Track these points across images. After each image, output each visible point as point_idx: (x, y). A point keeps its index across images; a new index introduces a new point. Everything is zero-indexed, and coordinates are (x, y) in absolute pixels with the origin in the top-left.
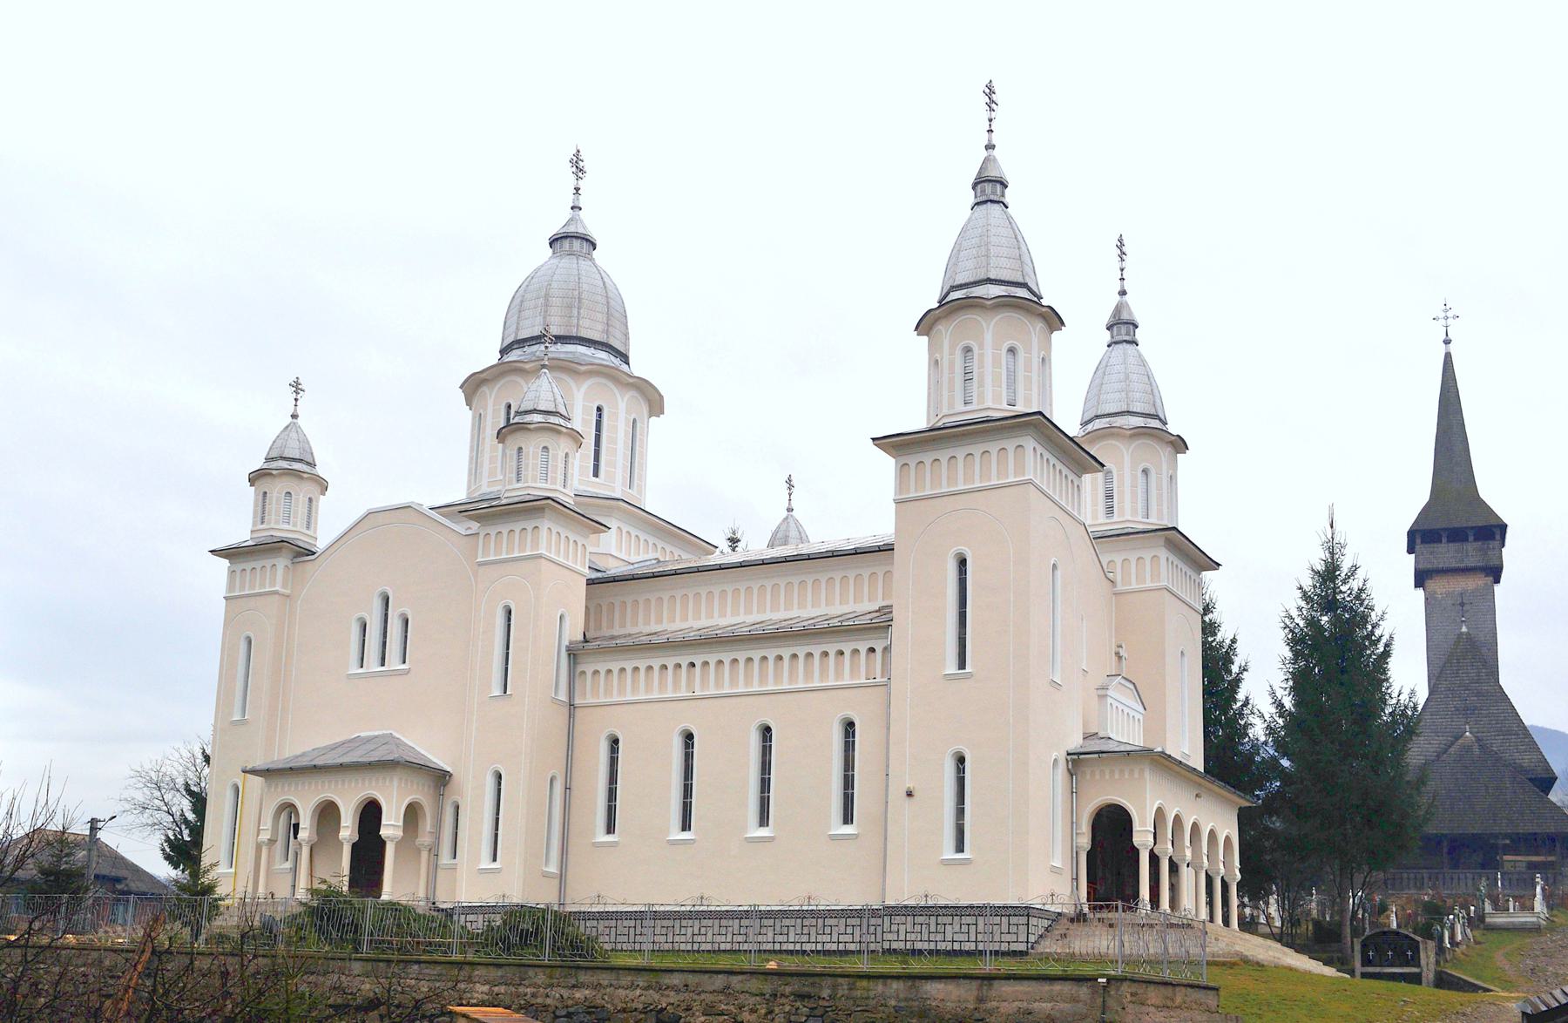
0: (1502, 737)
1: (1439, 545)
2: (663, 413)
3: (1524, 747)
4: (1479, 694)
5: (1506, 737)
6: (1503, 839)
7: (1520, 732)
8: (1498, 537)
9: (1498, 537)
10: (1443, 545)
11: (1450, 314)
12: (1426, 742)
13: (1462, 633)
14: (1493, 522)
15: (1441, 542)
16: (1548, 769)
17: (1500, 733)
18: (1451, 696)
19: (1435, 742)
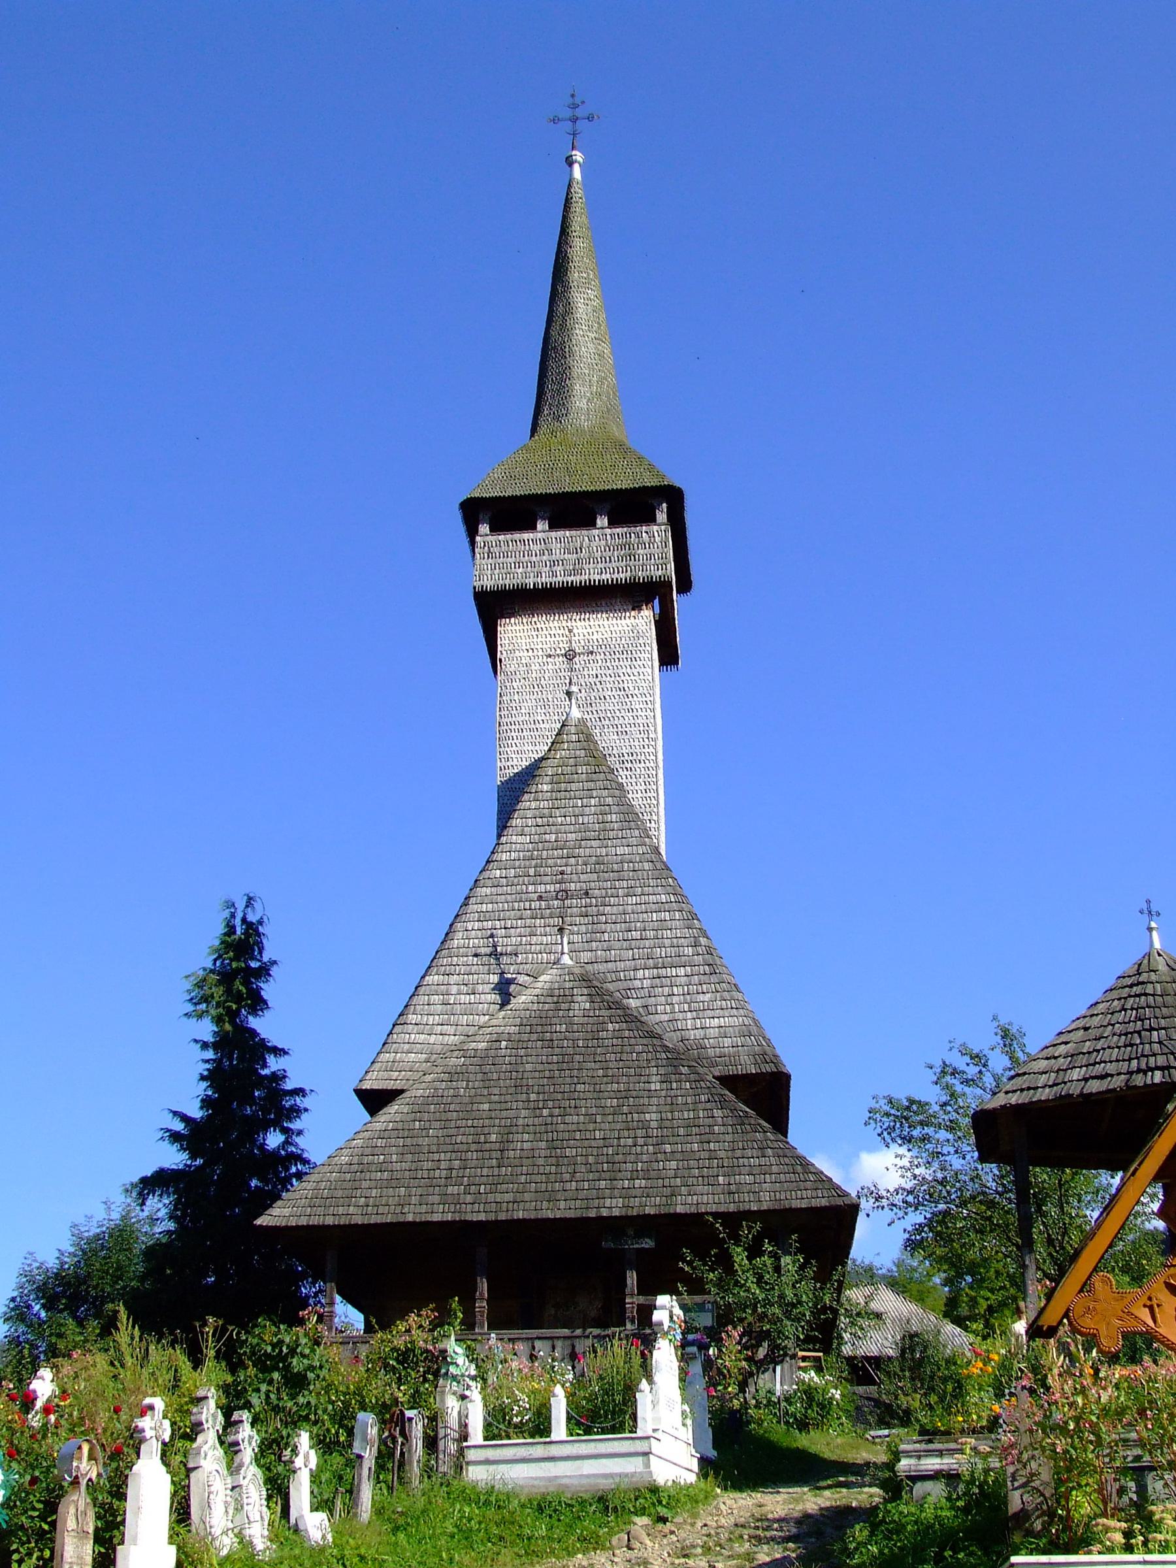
1: (526, 536)
5: (663, 972)
6: (640, 1235)
8: (662, 516)
9: (662, 516)
11: (579, 112)
16: (775, 1060)
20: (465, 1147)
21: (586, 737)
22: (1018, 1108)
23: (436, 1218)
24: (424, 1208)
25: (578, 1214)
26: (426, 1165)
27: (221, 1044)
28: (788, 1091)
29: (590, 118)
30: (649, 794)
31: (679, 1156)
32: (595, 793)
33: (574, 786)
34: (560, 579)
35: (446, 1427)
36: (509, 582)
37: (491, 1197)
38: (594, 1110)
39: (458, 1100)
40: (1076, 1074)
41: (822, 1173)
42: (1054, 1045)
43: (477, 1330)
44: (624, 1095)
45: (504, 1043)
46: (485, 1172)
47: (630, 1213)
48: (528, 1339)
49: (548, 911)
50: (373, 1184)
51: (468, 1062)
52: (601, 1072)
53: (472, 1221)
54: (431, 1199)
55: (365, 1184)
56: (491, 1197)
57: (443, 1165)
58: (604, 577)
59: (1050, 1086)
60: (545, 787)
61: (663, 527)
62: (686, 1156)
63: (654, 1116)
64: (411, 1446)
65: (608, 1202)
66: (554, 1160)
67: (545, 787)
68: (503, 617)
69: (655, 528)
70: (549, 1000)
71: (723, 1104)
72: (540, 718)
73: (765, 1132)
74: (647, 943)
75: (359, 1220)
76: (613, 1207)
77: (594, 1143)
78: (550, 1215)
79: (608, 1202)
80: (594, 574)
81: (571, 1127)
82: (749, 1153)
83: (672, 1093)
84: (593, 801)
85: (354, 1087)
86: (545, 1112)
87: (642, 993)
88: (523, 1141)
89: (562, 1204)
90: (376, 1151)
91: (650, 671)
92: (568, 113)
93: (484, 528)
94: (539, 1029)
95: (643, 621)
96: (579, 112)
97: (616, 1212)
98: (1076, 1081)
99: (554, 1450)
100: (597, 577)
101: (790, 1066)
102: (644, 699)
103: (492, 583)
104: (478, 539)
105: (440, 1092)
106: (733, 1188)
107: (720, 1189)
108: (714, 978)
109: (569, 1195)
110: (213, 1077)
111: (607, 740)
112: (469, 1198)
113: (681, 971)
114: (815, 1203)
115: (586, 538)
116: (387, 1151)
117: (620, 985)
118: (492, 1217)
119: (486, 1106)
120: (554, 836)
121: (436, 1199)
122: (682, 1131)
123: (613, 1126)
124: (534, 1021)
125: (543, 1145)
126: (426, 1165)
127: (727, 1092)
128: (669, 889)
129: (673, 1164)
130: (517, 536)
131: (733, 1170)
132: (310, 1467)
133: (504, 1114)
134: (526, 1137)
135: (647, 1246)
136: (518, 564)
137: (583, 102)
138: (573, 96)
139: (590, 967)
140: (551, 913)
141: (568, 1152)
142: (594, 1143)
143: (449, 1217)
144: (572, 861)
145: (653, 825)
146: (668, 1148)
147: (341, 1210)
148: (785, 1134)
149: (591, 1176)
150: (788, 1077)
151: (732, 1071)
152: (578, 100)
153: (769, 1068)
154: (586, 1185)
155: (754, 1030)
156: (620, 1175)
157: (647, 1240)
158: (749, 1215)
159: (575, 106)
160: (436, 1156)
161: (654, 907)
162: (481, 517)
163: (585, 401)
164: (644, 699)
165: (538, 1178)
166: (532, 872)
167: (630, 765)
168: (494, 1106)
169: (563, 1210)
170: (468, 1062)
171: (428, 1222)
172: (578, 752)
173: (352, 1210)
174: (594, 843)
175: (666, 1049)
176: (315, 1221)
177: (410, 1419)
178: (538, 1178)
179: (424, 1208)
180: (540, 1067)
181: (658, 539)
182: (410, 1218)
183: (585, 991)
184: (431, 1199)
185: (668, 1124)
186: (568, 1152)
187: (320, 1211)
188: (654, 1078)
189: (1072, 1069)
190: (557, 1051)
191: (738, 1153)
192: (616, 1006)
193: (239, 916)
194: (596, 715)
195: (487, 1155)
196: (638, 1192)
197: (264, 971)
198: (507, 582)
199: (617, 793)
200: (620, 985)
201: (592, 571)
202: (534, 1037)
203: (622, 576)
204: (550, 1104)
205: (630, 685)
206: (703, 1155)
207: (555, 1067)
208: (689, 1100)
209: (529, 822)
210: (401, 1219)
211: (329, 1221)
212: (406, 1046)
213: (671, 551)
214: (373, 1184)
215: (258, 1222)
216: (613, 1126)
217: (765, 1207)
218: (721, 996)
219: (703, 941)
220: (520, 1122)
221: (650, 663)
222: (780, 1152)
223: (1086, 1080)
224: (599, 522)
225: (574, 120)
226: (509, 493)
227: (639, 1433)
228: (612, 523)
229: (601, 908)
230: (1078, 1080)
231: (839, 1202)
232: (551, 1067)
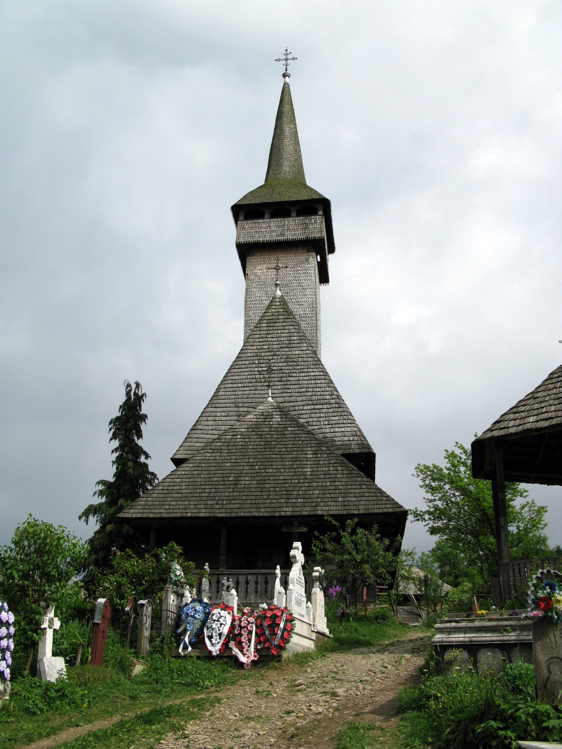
3: (336, 418)
4: (288, 359)
5: (316, 407)
6: (300, 525)
7: (333, 401)
8: (321, 213)
10: (265, 220)
11: (289, 57)
12: (223, 414)
14: (315, 197)
16: (368, 447)
17: (310, 402)
20: (217, 483)
21: (283, 302)
22: (499, 437)
23: (202, 515)
24: (196, 511)
25: (270, 514)
26: (198, 491)
27: (121, 447)
28: (374, 463)
29: (293, 59)
30: (313, 332)
31: (319, 488)
32: (287, 328)
33: (277, 324)
34: (274, 238)
35: (167, 610)
36: (251, 240)
37: (228, 506)
38: (280, 467)
39: (216, 461)
40: (531, 419)
41: (389, 496)
42: (517, 407)
43: (220, 570)
44: (296, 459)
45: (239, 436)
46: (226, 494)
47: (295, 514)
48: (245, 574)
49: (263, 379)
50: (173, 499)
51: (222, 444)
52: (284, 450)
53: (219, 517)
54: (200, 506)
55: (169, 499)
56: (228, 506)
57: (207, 491)
58: (294, 237)
59: (516, 426)
60: (264, 325)
61: (321, 217)
62: (324, 488)
63: (309, 470)
64: (142, 621)
65: (284, 509)
66: (259, 489)
67: (264, 325)
68: (249, 255)
69: (317, 217)
70: (261, 417)
71: (342, 464)
72: (264, 299)
73: (362, 477)
74: (309, 394)
75: (164, 515)
76: (287, 511)
77: (279, 482)
78: (256, 514)
79: (284, 509)
80: (289, 236)
81: (268, 474)
82: (354, 487)
83: (318, 459)
84: (286, 331)
85: (171, 457)
86: (257, 467)
87: (305, 416)
88: (245, 481)
89: (262, 510)
90: (176, 484)
91: (314, 278)
92: (284, 57)
93: (241, 217)
94: (256, 430)
95: (314, 260)
96: (289, 57)
97: (288, 514)
98: (531, 422)
100: (291, 238)
101: (375, 451)
102: (311, 290)
103: (244, 241)
104: (239, 222)
105: (208, 458)
106: (346, 503)
107: (339, 504)
108: (340, 410)
109: (266, 505)
110: (120, 461)
111: (293, 307)
112: (218, 506)
113: (325, 406)
114: (385, 511)
115: (287, 222)
116: (181, 484)
117: (296, 413)
118: (229, 515)
119: (229, 464)
120: (267, 346)
121: (202, 506)
122: (322, 477)
123: (289, 474)
124: (254, 426)
125: (255, 482)
126: (198, 491)
127: (344, 459)
128: (320, 370)
129: (317, 492)
130: (255, 221)
131: (345, 495)
132: (54, 627)
133: (237, 468)
134: (247, 478)
135: (304, 531)
136: (256, 232)
137: (290, 53)
138: (286, 50)
139: (281, 404)
140: (264, 380)
141: (266, 486)
142: (279, 482)
143: (208, 515)
144: (275, 357)
145: (314, 345)
146: (315, 484)
147: (157, 511)
148: (374, 481)
149: (277, 497)
150: (374, 455)
151: (347, 451)
152: (288, 52)
153: (365, 450)
154: (275, 501)
155: (358, 433)
156: (291, 497)
157: (304, 528)
158: (352, 516)
159: (287, 54)
160: (204, 487)
161: (313, 378)
162: (240, 213)
163: (288, 167)
164: (311, 290)
165: (251, 498)
166: (257, 362)
167: (304, 319)
168: (233, 464)
169: (263, 513)
170: (222, 444)
171: (198, 517)
172: (280, 310)
173: (162, 511)
174: (286, 350)
175: (316, 439)
176: (145, 515)
177: (142, 605)
178: (251, 498)
179: (196, 511)
180: (256, 447)
181: (318, 221)
182: (189, 515)
183: (279, 413)
184: (200, 506)
185: (315, 473)
186: (266, 486)
187: (147, 511)
188: (309, 453)
189: (528, 417)
190: (264, 440)
191: (349, 487)
192: (294, 421)
193: (133, 391)
194: (289, 297)
195: (228, 486)
196: (299, 505)
197: (144, 418)
198: (251, 240)
199: (297, 327)
200: (296, 413)
201: (289, 235)
202: (254, 433)
203: (302, 237)
204: (259, 464)
205: (305, 285)
206: (331, 488)
207: (263, 447)
208: (326, 462)
209: (256, 340)
210: (185, 515)
211: (151, 516)
212: (196, 440)
213: (325, 234)
214: (173, 499)
215: (118, 516)
216: (289, 474)
217: (361, 512)
218: (343, 418)
219: (335, 393)
220: (245, 471)
221: (314, 275)
222: (369, 487)
223: (537, 421)
225: (287, 59)
226: (253, 202)
228: (298, 215)
229: (288, 378)
230: (532, 422)
231: (398, 510)
232: (260, 447)
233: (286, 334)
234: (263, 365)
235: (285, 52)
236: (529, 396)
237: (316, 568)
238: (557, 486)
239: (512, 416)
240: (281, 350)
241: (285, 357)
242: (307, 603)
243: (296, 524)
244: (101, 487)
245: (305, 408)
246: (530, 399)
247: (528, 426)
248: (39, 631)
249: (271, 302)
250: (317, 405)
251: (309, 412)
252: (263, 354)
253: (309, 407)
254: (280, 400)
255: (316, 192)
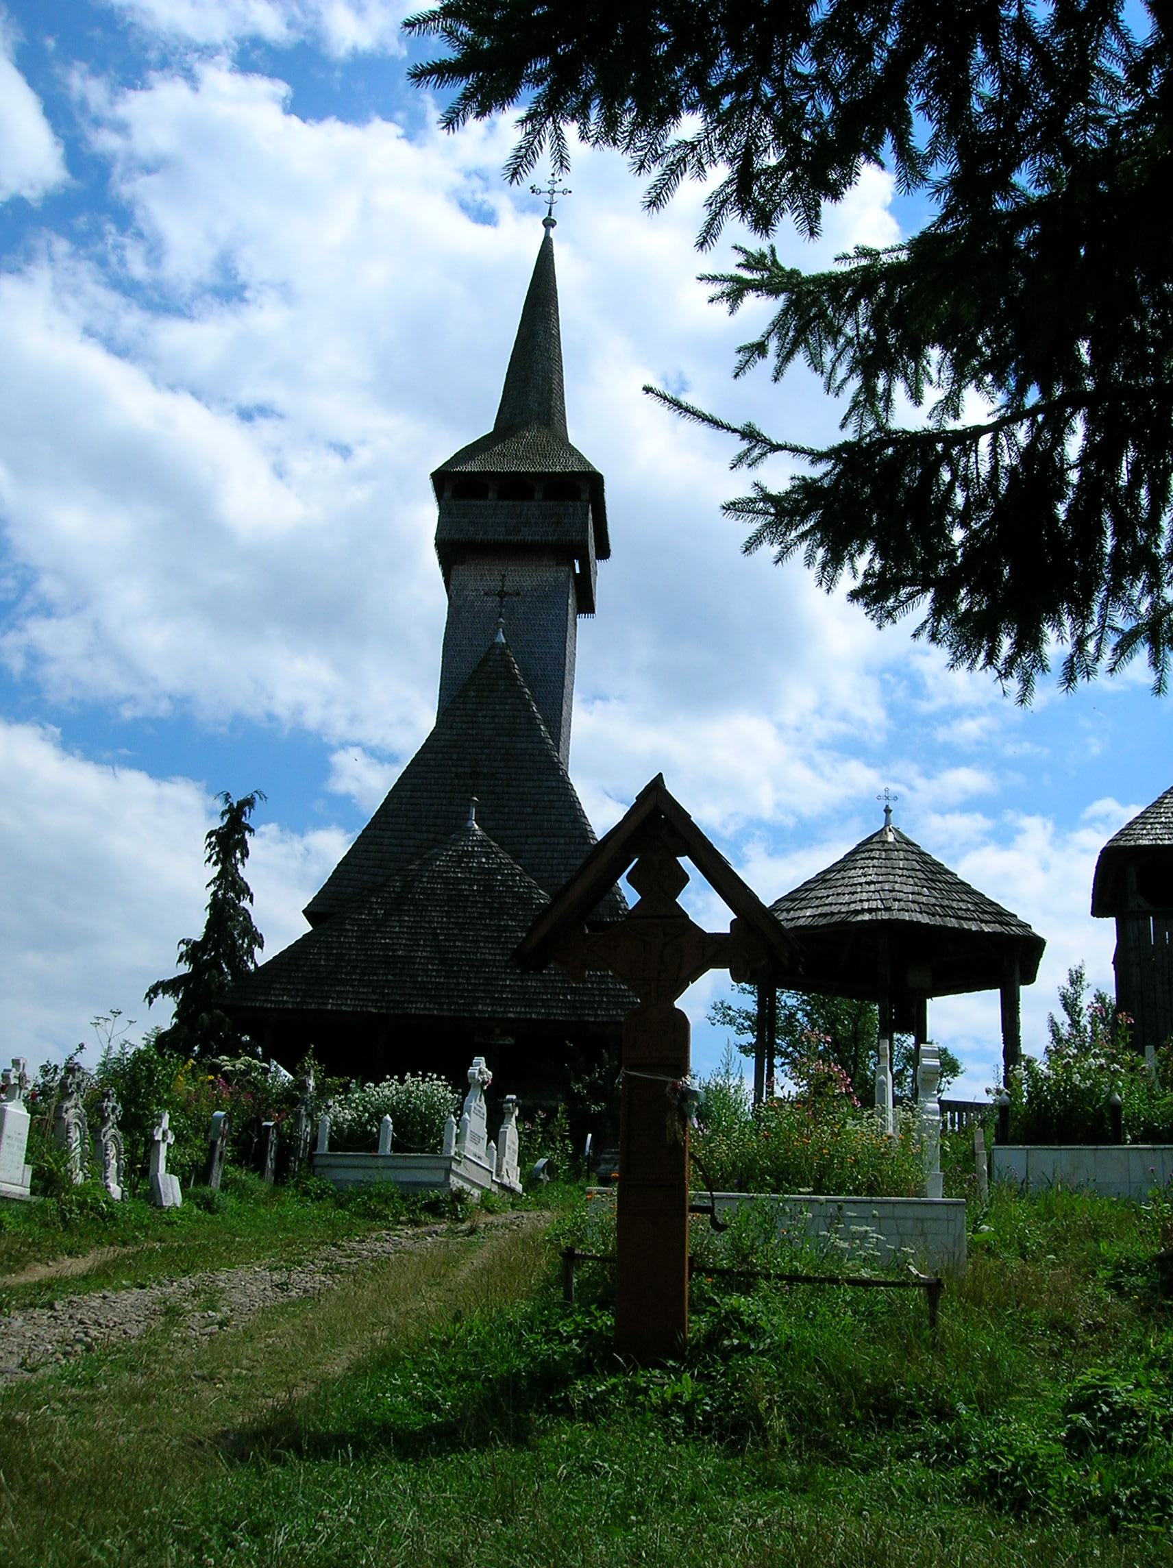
0: (541, 840)
2: (304, 912)
10: (488, 503)
11: (557, 187)
13: (494, 645)
15: (485, 497)
18: (455, 756)
19: (412, 842)
92: (549, 187)
96: (557, 187)
99: (381, 1162)
166: (455, 756)
224: (490, 495)
227: (379, 1154)
228: (546, 498)
233: (507, 713)
234: (466, 763)
235: (551, 178)
236: (820, 877)
237: (508, 1097)
238: (965, 994)
239: (788, 904)
240: (497, 739)
241: (502, 751)
242: (488, 1142)
243: (497, 1031)
244: (183, 948)
245: (530, 840)
246: (818, 881)
247: (801, 922)
248: (152, 1145)
249: (488, 654)
250: (550, 837)
251: (534, 847)
252: (467, 744)
253: (535, 840)
254: (491, 824)
255: (581, 459)
